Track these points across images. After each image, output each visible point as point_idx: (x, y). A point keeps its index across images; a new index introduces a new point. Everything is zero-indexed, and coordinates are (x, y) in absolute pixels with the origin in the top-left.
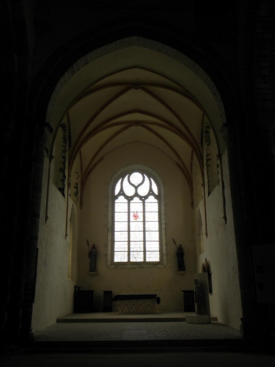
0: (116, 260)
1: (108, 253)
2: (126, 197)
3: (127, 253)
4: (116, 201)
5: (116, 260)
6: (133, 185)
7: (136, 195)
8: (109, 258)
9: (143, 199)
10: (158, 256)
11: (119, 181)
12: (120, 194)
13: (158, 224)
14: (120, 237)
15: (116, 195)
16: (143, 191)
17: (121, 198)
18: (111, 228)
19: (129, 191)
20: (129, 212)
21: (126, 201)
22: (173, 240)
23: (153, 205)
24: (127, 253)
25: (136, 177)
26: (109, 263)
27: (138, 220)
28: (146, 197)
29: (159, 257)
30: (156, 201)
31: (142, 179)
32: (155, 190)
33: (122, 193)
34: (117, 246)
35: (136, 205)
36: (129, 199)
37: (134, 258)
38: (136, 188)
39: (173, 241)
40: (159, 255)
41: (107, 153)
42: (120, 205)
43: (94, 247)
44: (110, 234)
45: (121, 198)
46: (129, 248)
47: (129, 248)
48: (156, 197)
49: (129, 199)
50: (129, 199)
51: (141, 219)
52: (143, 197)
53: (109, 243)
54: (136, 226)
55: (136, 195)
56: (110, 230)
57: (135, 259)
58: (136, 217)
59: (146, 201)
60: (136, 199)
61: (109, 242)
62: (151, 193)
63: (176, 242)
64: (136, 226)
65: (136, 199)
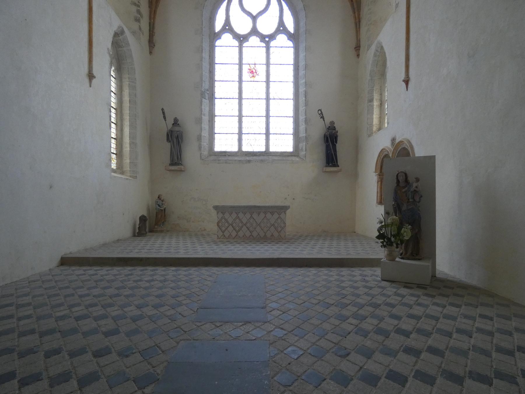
1: (203, 134)
4: (218, 43)
6: (249, 14)
7: (254, 31)
8: (205, 143)
9: (267, 40)
11: (222, 6)
16: (267, 24)
19: (242, 25)
21: (236, 43)
22: (320, 112)
23: (284, 51)
26: (205, 153)
27: (257, 78)
28: (272, 37)
30: (291, 44)
33: (228, 27)
35: (254, 51)
36: (242, 39)
42: (225, 50)
43: (176, 122)
44: (206, 102)
45: (227, 39)
49: (227, 28)
50: (242, 39)
51: (262, 76)
53: (205, 118)
54: (254, 89)
55: (254, 31)
60: (254, 40)
61: (204, 115)
62: (281, 28)
64: (254, 89)
65: (254, 40)
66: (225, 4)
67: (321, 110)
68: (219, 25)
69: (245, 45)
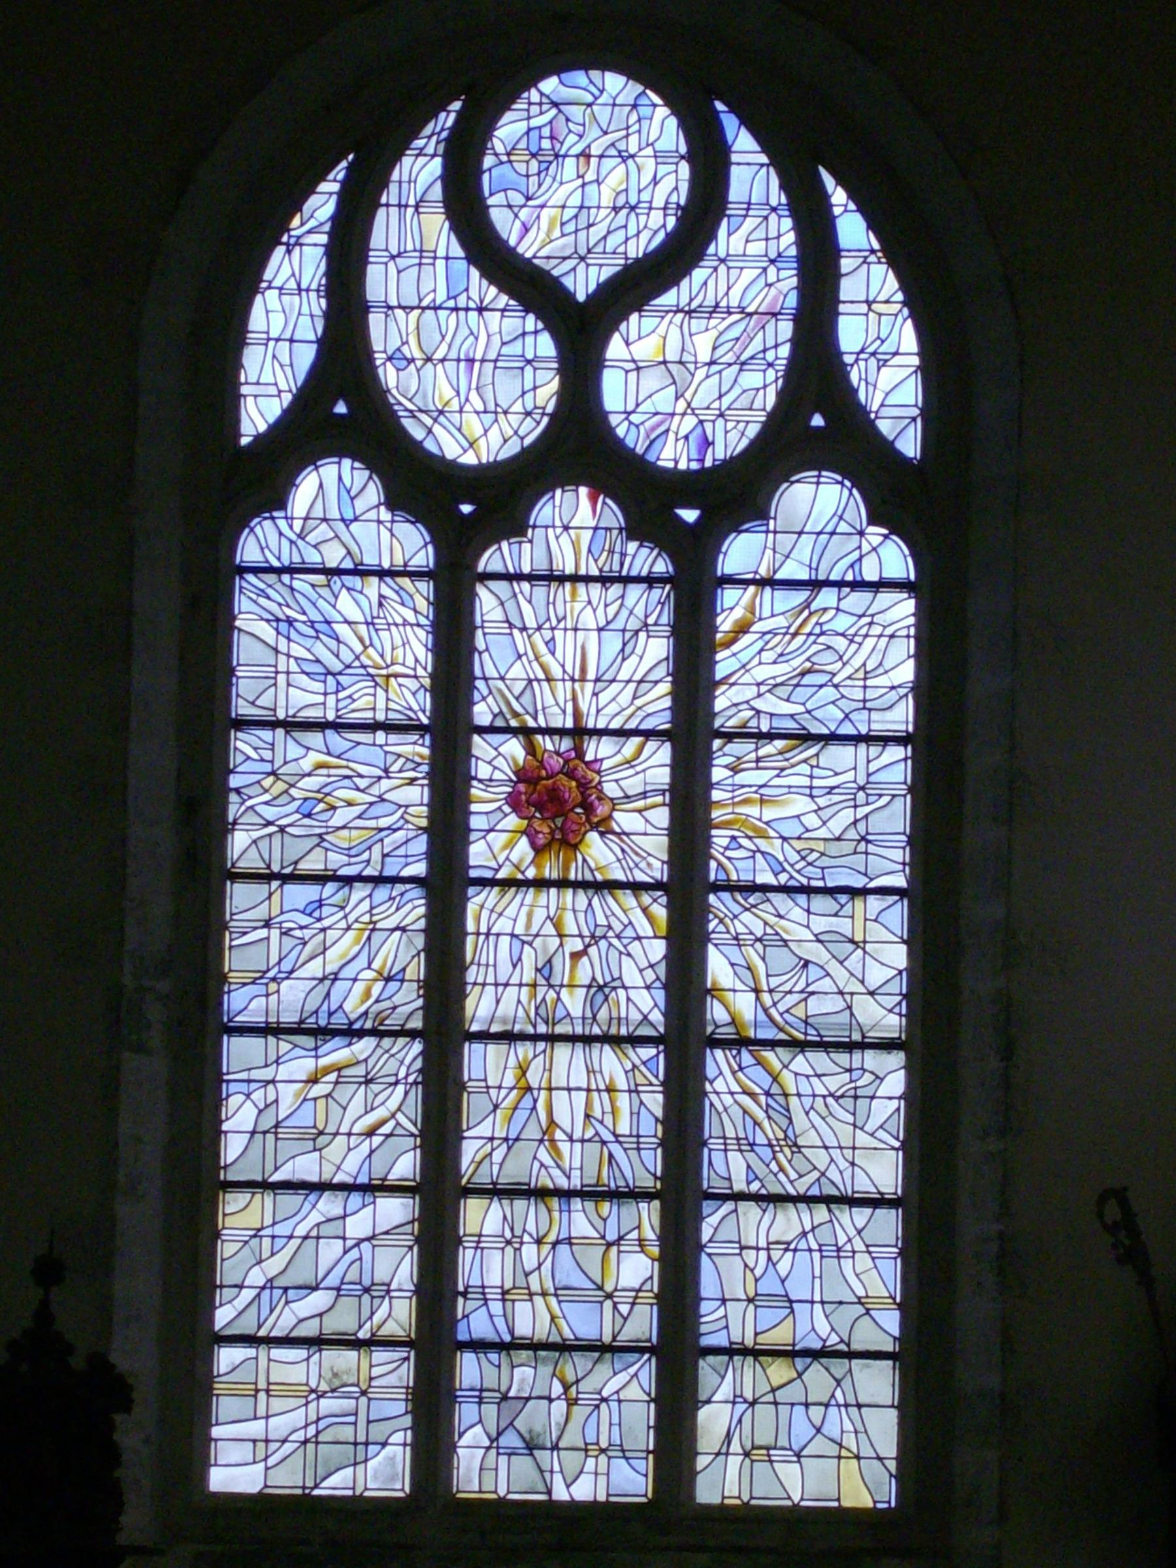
0: (233, 1473)
2: (417, 482)
3: (394, 1372)
5: (233, 1473)
6: (529, 286)
7: (577, 446)
9: (686, 520)
10: (884, 1431)
12: (310, 431)
13: (896, 1420)
14: (310, 1119)
15: (244, 441)
16: (689, 380)
17: (332, 495)
18: (164, 986)
19: (472, 387)
20: (449, 730)
22: (1112, 1211)
23: (833, 622)
24: (405, 1374)
25: (594, 159)
27: (598, 852)
28: (739, 491)
29: (889, 1447)
30: (894, 559)
31: (674, 183)
32: (891, 385)
33: (346, 407)
34: (254, 1252)
35: (574, 635)
36: (465, 513)
37: (510, 1440)
38: (579, 330)
39: (1112, 1229)
40: (891, 1417)
41: (839, 1046)
42: (322, 609)
44: (146, 1072)
45: (332, 495)
46: (437, 1288)
47: (437, 1288)
48: (892, 493)
50: (465, 513)
51: (639, 838)
52: (685, 486)
53: (139, 1219)
54: (557, 946)
55: (577, 446)
56: (155, 1013)
57: (523, 1464)
58: (559, 802)
59: (740, 553)
60: (572, 522)
62: (815, 418)
63: (324, 994)
64: (557, 946)
65: (572, 522)
66: (322, 204)
67: (1121, 1195)
68: (269, 382)
69: (490, 560)
